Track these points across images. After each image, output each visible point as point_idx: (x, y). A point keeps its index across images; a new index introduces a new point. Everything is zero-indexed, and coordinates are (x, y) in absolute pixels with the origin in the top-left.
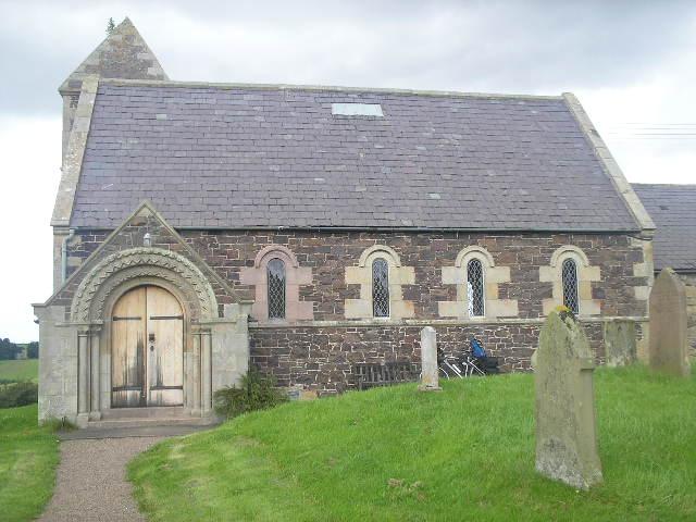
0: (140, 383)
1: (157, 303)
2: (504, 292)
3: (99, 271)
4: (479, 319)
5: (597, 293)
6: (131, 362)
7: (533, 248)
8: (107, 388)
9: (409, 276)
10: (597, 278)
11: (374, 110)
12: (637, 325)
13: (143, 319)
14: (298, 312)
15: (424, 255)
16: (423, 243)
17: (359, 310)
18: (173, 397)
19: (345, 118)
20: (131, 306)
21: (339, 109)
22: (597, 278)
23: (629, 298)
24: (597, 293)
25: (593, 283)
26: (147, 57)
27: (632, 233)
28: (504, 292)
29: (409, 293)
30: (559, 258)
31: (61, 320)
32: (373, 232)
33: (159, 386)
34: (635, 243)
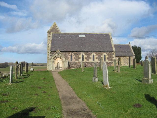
0: (58, 67)
1: (59, 59)
2: (97, 58)
3: (54, 56)
4: (71, 61)
5: (108, 59)
6: (57, 65)
7: (101, 53)
8: (54, 67)
9: (86, 56)
10: (108, 57)
11: (84, 36)
12: (112, 62)
13: (59, 62)
14: (74, 60)
15: (88, 54)
16: (88, 53)
17: (91, 60)
18: (61, 68)
19: (81, 37)
20: (57, 59)
21: (80, 36)
22: (108, 57)
23: (112, 59)
24: (108, 59)
25: (107, 57)
26: (57, 28)
27: (113, 52)
28: (97, 58)
29: (86, 58)
30: (103, 54)
31: (50, 61)
32: (82, 52)
33: (59, 67)
34: (113, 53)
